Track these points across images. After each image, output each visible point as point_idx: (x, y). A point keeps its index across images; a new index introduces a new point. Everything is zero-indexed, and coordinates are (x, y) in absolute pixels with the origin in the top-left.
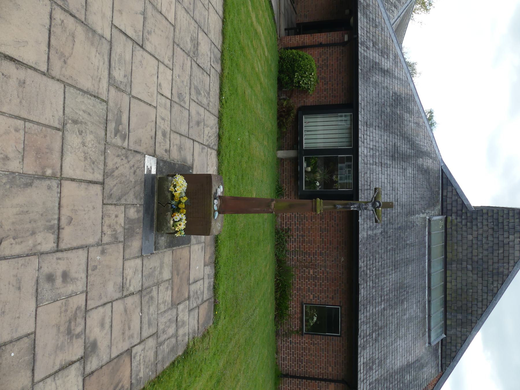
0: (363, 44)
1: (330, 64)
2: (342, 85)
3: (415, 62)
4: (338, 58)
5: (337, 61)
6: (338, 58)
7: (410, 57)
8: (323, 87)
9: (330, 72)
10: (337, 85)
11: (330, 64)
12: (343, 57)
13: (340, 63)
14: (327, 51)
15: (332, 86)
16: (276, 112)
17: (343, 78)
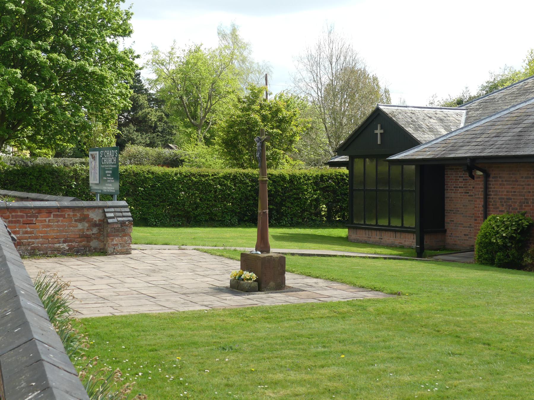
0: (355, 123)
1: (506, 195)
2: (530, 178)
3: (216, 31)
4: (500, 184)
5: (504, 185)
6: (500, 184)
7: (245, 41)
8: (530, 206)
9: (515, 195)
10: (529, 185)
11: (506, 195)
12: (500, 177)
13: (506, 181)
14: (492, 198)
15: (530, 192)
16: (499, 269)
17: (522, 177)
